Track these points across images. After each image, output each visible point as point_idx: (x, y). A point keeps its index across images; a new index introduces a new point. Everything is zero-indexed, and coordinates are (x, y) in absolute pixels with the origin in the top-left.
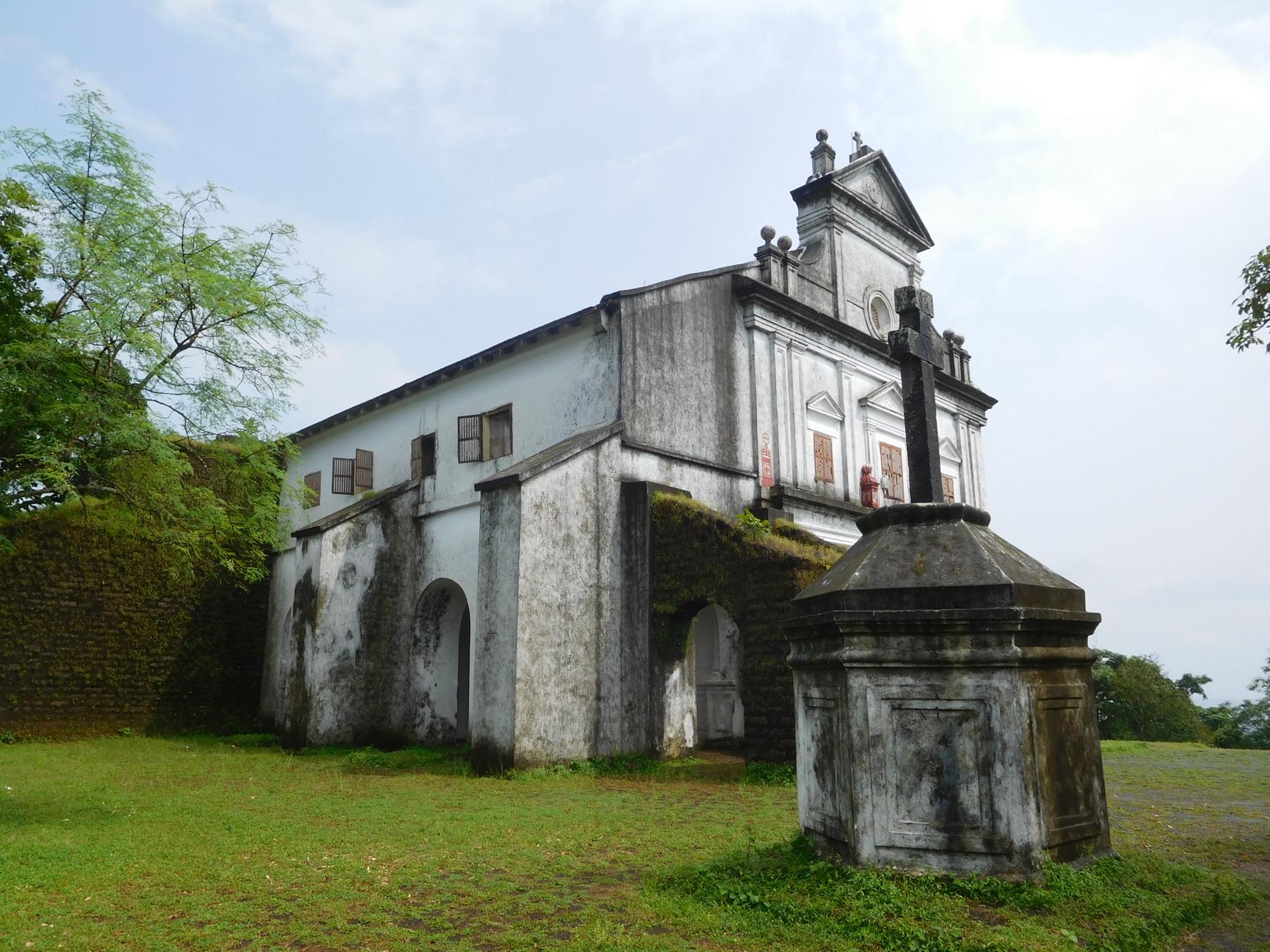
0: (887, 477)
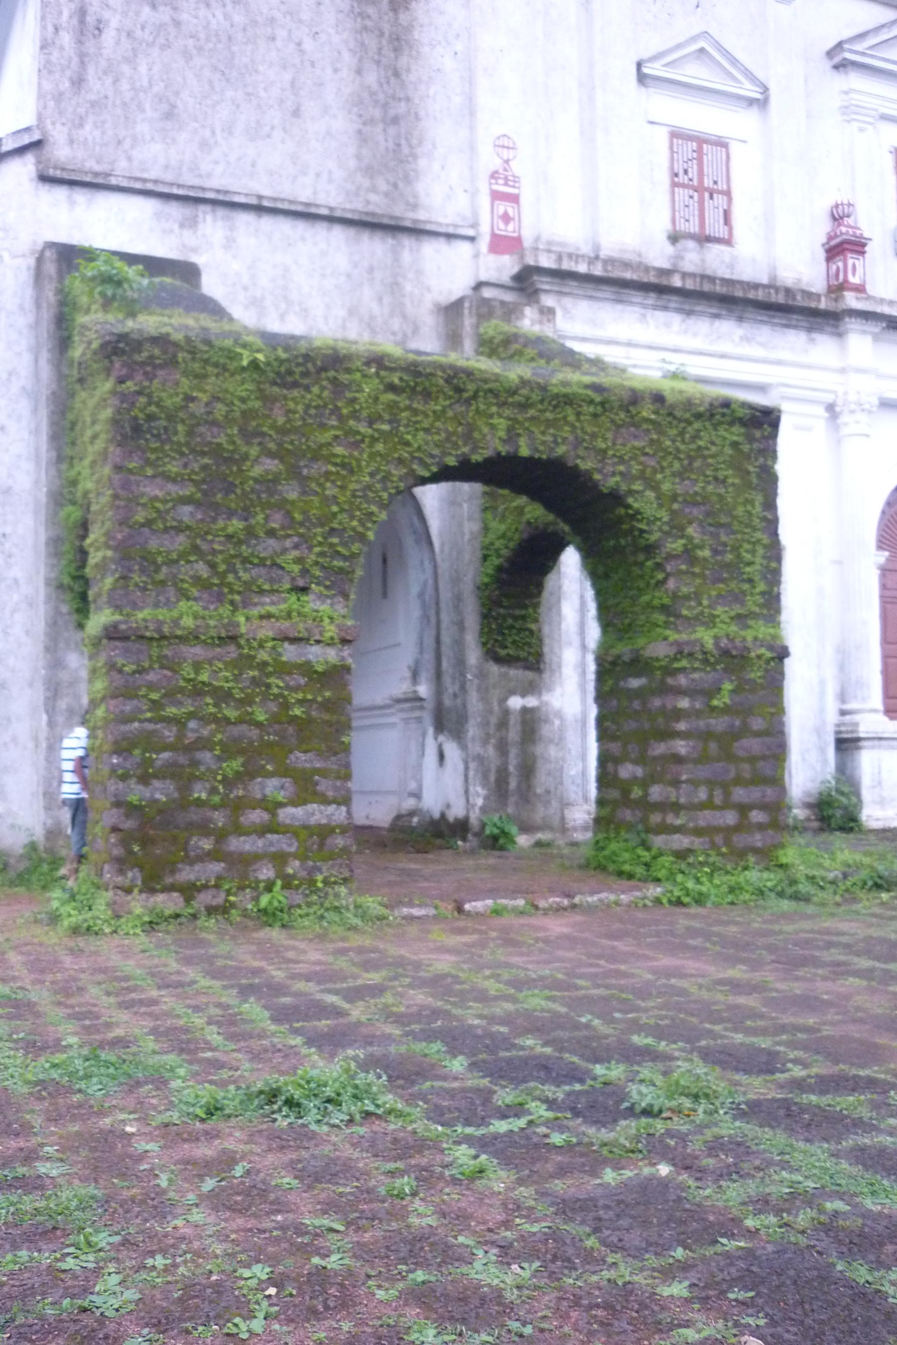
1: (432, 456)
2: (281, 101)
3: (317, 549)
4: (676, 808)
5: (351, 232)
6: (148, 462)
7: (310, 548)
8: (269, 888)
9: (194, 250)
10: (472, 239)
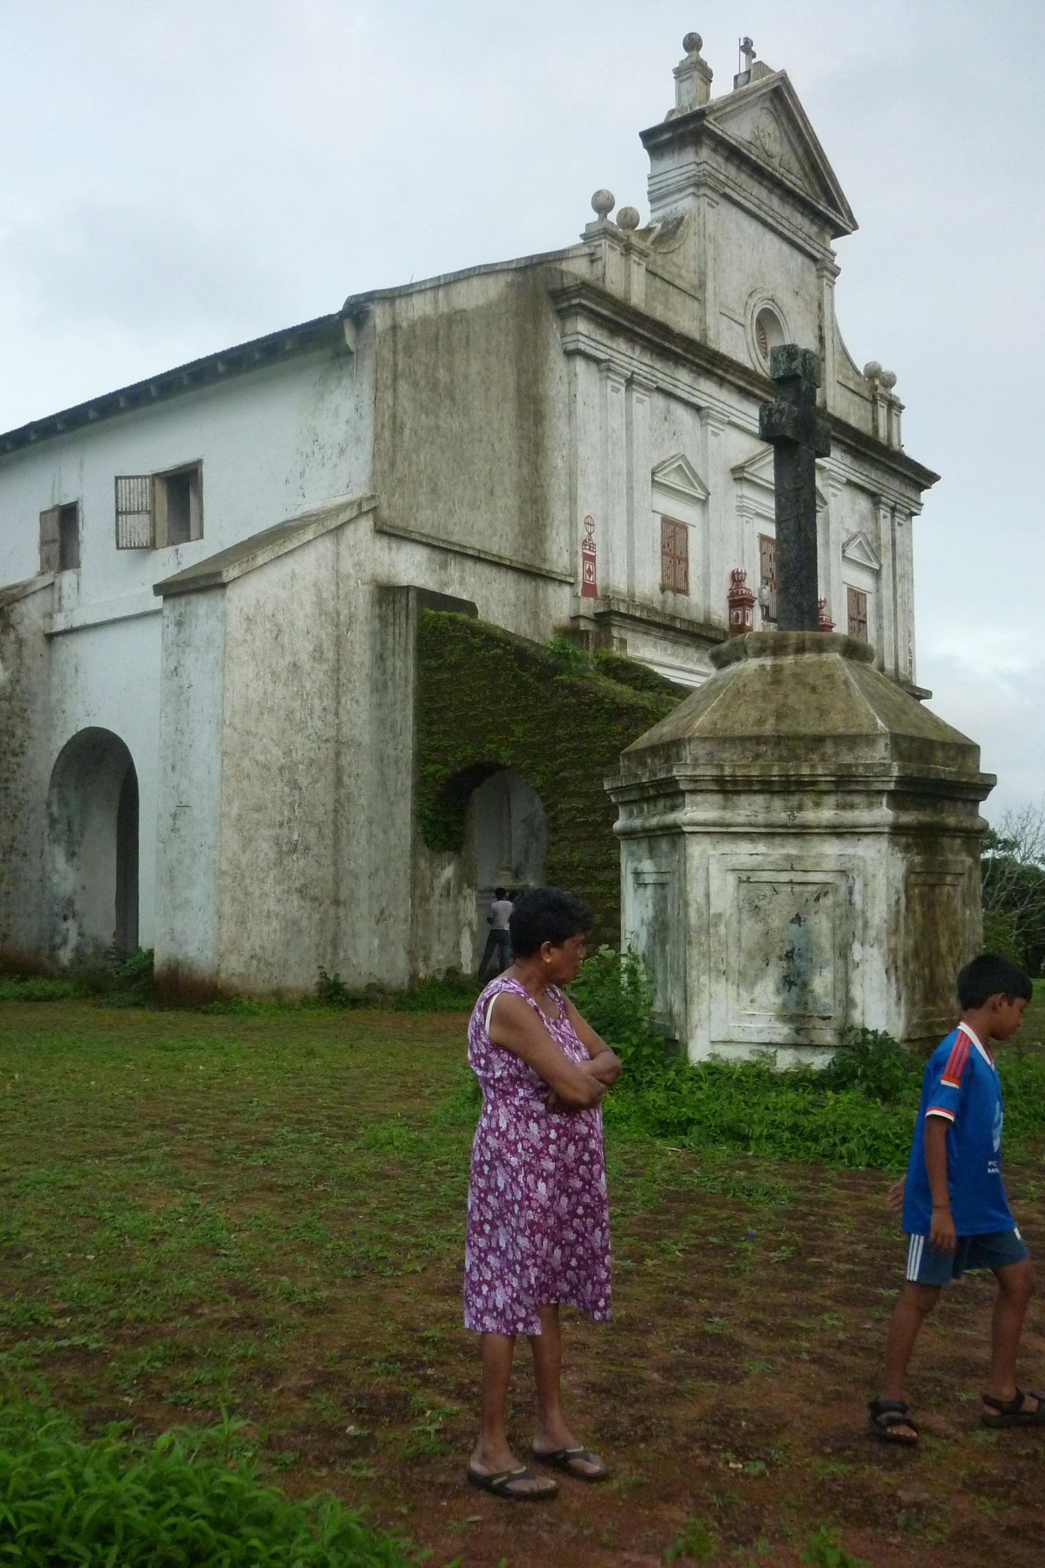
0: (768, 588)
2: (485, 485)
10: (571, 584)
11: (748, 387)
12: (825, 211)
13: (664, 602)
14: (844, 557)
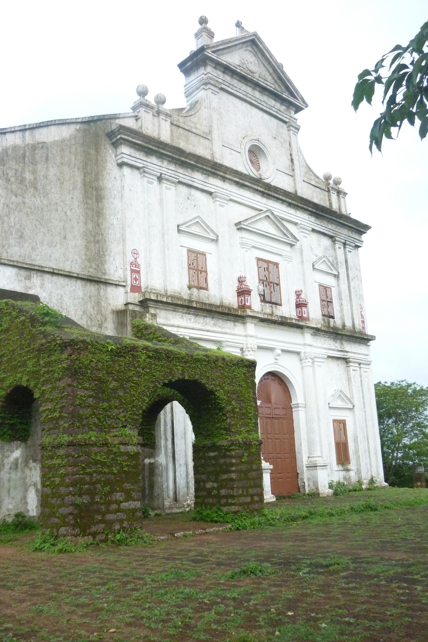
1: (161, 380)
2: (60, 233)
3: (129, 413)
4: (233, 497)
5: (84, 282)
6: (79, 383)
7: (127, 412)
8: (119, 533)
9: (30, 288)
10: (124, 286)
11: (241, 181)
12: (287, 98)
13: (191, 294)
14: (314, 269)
